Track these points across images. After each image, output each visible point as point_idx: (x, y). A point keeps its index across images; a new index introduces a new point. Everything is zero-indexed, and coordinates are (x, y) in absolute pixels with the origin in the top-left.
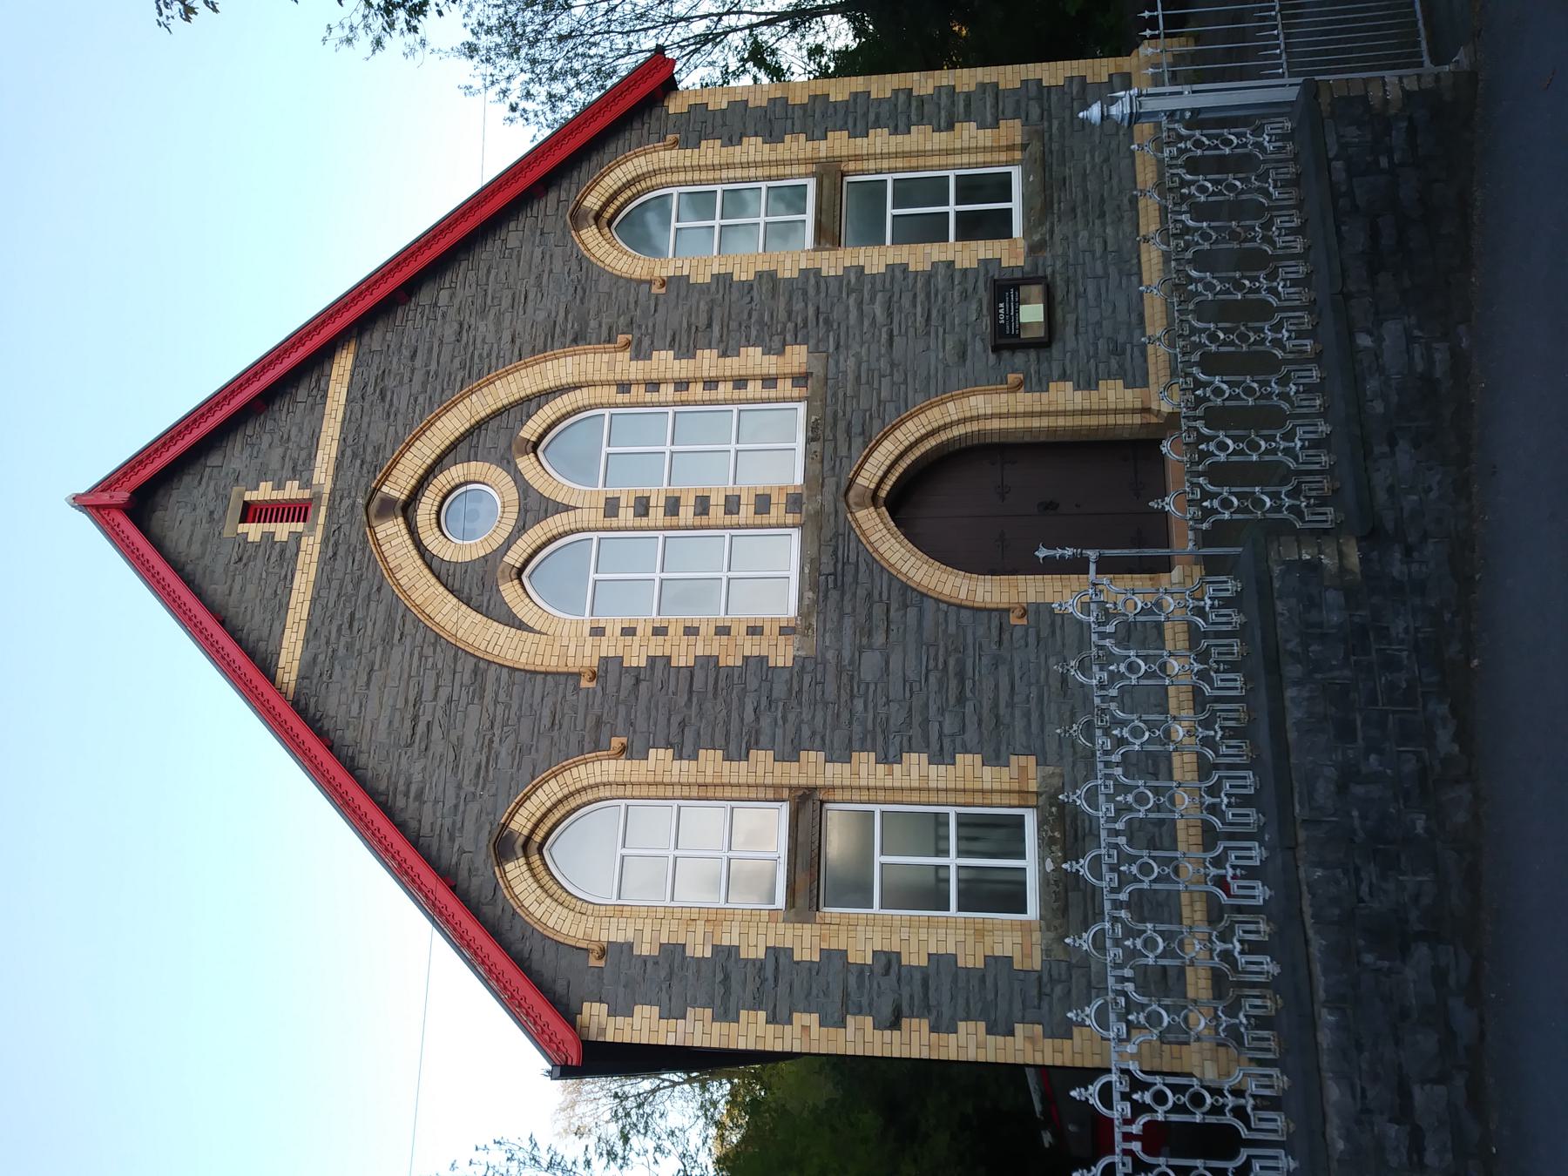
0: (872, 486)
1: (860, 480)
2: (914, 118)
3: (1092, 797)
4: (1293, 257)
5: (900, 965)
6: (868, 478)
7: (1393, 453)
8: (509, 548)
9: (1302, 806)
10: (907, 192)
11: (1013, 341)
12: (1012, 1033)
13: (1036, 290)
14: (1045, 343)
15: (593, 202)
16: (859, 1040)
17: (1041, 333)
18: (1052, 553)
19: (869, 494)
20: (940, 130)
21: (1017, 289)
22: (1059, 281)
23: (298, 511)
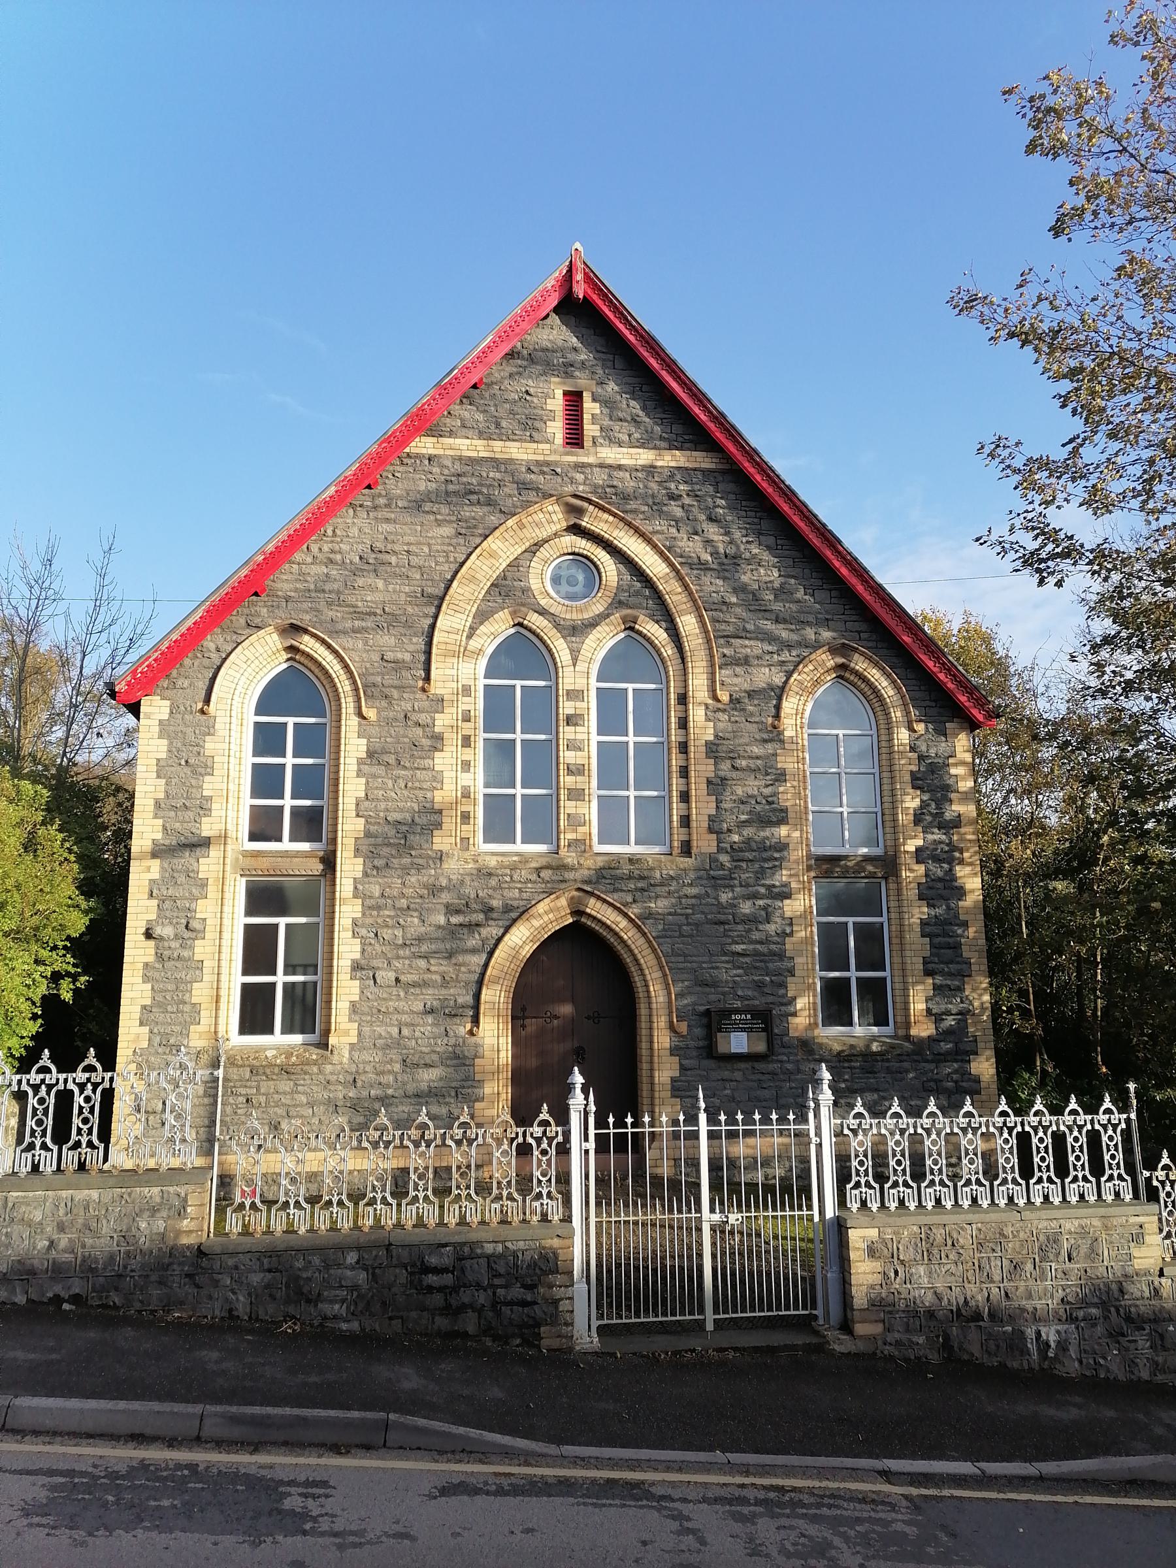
0: (588, 910)
1: (592, 901)
2: (937, 940)
3: (90, 1069)
4: (441, 1216)
5: (194, 940)
6: (594, 907)
7: (264, 1271)
8: (540, 614)
9: (17, 1197)
10: (870, 938)
11: (714, 1026)
12: (141, 1024)
13: (761, 1047)
14: (709, 1051)
15: (860, 664)
16: (139, 910)
17: (722, 1049)
18: (1132, 1095)
19: (582, 908)
20: (925, 963)
21: (764, 1030)
22: (772, 1067)
23: (575, 438)
